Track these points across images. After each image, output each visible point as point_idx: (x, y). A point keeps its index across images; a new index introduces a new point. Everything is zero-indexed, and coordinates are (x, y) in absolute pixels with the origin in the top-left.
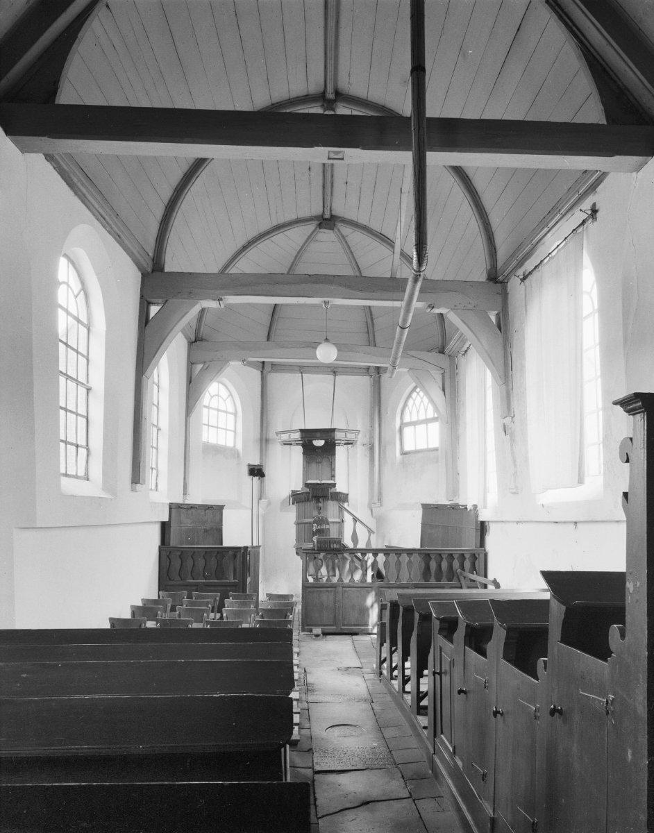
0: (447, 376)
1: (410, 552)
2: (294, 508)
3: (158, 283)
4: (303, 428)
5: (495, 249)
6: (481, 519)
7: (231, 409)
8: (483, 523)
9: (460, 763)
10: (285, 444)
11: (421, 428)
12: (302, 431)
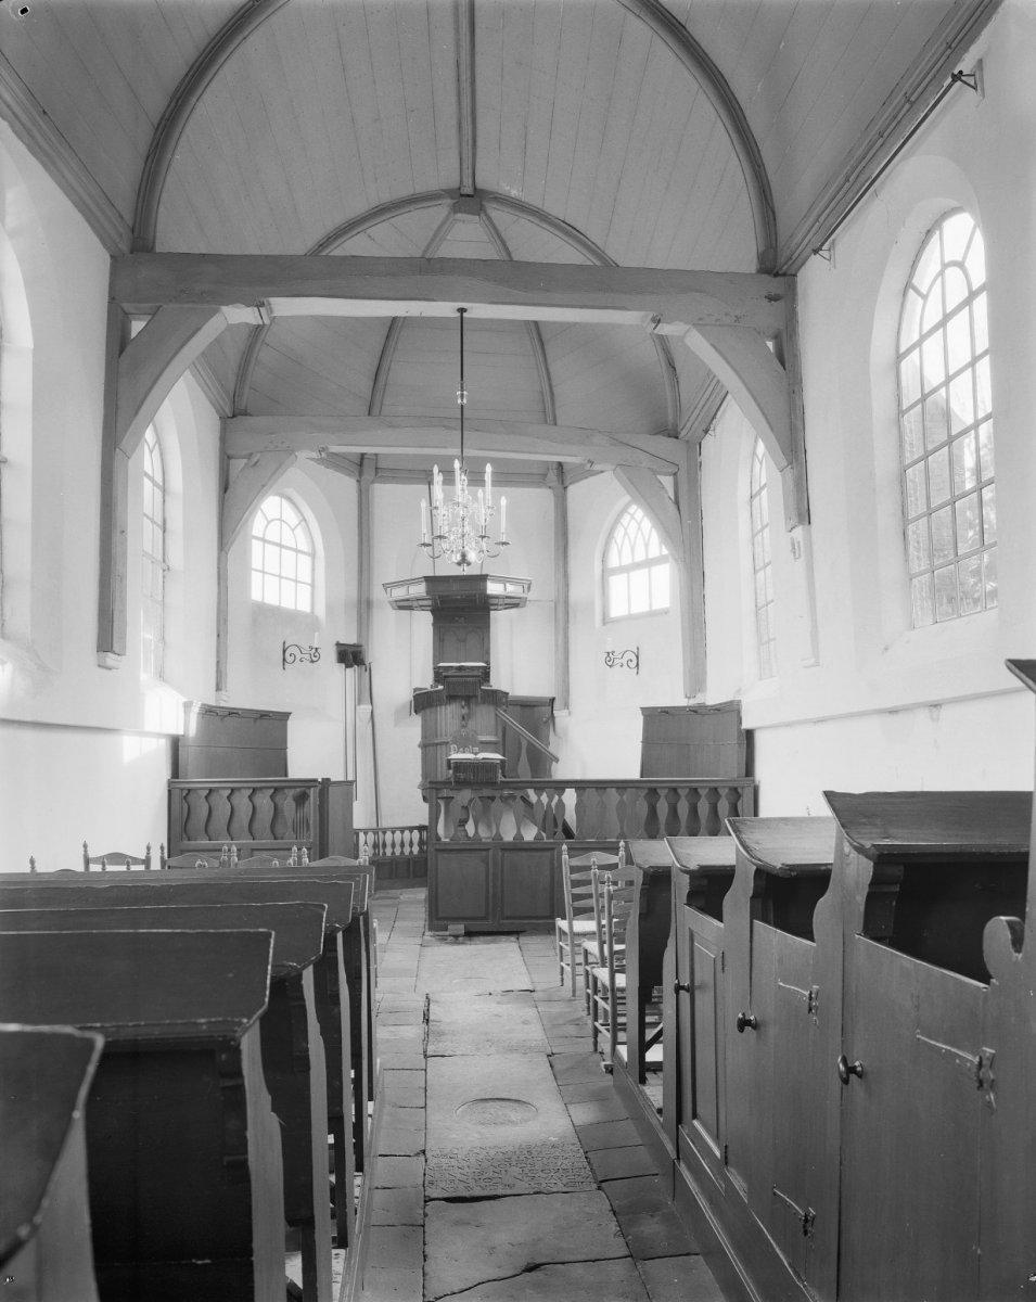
0: (682, 475)
1: (622, 785)
2: (417, 720)
4: (430, 574)
5: (774, 213)
6: (746, 725)
7: (304, 546)
8: (750, 734)
9: (739, 1183)
10: (401, 608)
11: (639, 576)
12: (427, 579)
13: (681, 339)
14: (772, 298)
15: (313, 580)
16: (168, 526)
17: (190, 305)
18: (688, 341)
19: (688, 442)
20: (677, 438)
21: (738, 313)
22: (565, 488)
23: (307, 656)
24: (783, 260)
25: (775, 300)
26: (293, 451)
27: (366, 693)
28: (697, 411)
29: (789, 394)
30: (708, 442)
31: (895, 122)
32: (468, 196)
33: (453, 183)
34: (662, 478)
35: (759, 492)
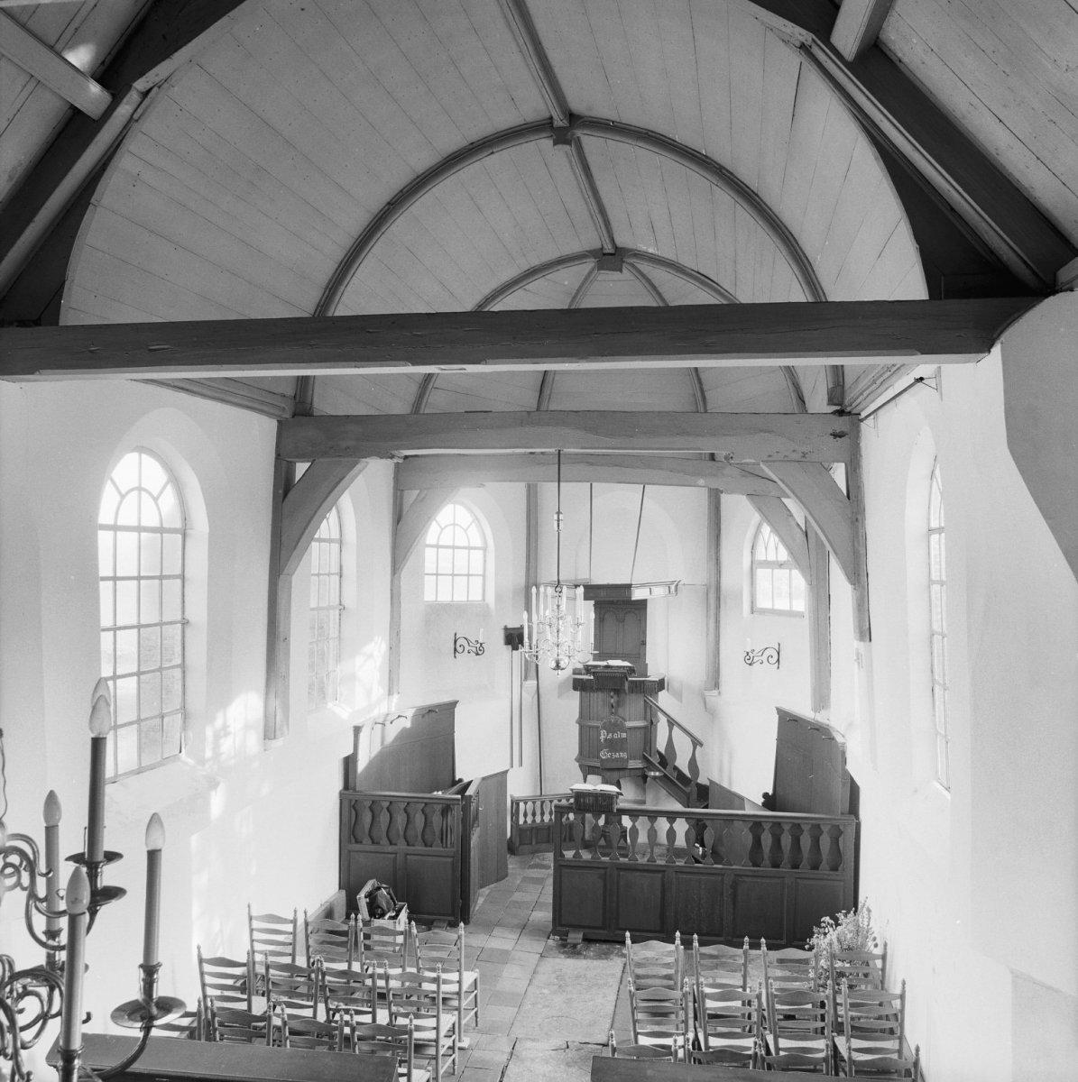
7: (477, 542)
14: (836, 435)
15: (485, 571)
17: (337, 459)
23: (474, 649)
25: (840, 437)
27: (531, 670)
29: (852, 522)
32: (611, 254)
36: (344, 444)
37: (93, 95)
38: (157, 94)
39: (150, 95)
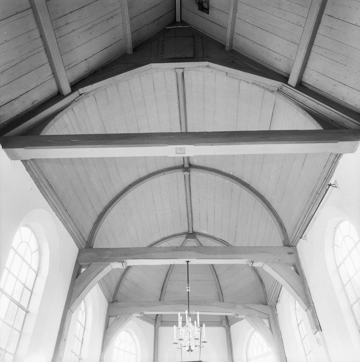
0: (271, 319)
3: (89, 256)
13: (262, 268)
16: (84, 342)
18: (264, 268)
19: (271, 306)
20: (267, 305)
21: (279, 258)
22: (230, 326)
24: (291, 242)
26: (132, 314)
28: (272, 295)
30: (278, 306)
31: (315, 200)
32: (191, 234)
33: (187, 230)
34: (263, 320)
35: (300, 323)
36: (104, 258)
37: (66, 89)
38: (84, 96)
39: (82, 95)
